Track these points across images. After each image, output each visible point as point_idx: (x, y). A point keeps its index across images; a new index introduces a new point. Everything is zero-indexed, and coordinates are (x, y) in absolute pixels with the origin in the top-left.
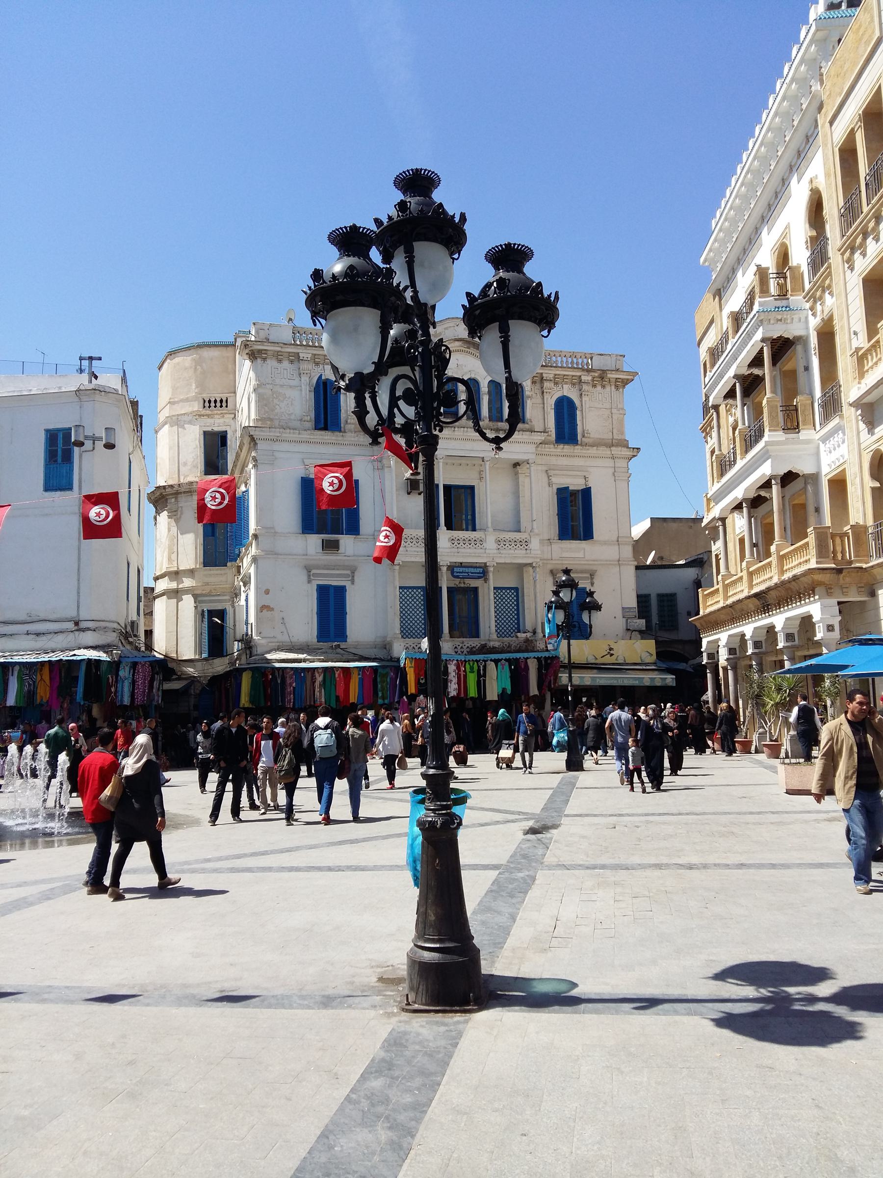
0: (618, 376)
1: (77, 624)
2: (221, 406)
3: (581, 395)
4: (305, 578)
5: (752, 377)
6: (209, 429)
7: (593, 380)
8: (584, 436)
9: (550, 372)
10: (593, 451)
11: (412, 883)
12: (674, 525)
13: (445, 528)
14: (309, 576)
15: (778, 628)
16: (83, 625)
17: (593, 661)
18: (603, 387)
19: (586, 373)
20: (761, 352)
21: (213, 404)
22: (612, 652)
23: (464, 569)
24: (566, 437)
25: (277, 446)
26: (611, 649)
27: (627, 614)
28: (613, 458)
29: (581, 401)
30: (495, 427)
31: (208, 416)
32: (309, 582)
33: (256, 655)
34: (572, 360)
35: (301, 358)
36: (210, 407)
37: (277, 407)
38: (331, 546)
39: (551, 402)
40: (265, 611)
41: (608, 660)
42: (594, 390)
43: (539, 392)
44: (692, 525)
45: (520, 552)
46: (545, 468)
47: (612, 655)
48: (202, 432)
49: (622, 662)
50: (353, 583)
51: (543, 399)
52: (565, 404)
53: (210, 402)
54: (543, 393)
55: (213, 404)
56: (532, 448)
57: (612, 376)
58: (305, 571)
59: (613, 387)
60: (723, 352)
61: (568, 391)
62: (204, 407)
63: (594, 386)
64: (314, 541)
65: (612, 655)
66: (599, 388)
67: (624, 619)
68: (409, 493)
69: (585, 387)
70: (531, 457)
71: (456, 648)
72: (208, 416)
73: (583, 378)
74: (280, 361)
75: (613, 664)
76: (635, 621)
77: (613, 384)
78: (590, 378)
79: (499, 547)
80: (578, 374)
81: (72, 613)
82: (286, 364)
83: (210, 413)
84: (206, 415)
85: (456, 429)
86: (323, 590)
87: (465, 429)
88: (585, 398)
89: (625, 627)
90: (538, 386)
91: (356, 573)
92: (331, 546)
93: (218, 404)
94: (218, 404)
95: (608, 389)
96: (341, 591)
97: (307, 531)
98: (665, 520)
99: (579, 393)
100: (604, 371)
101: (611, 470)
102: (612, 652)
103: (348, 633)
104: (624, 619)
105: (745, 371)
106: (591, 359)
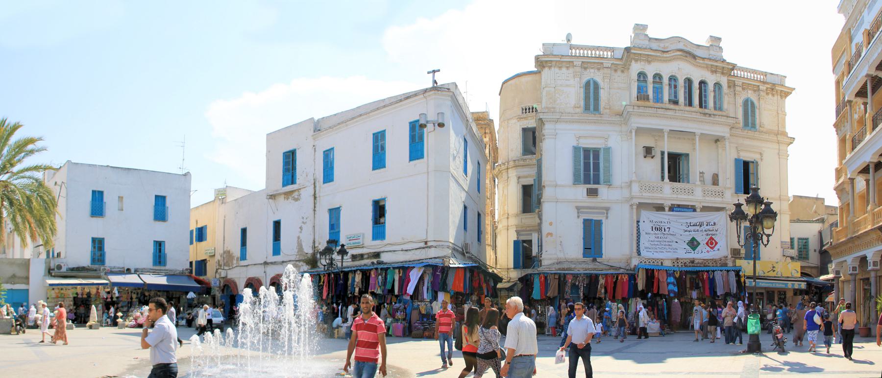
0: (783, 89)
1: (426, 243)
2: (533, 112)
3: (759, 98)
4: (576, 215)
5: (878, 78)
6: (526, 127)
7: (767, 90)
8: (760, 126)
9: (740, 80)
10: (766, 136)
11: (876, 66)
12: (806, 201)
13: (668, 180)
14: (578, 213)
15: (870, 258)
16: (429, 244)
17: (762, 275)
18: (773, 95)
19: (763, 84)
20: (865, 85)
21: (527, 111)
22: (774, 269)
23: (681, 209)
24: (750, 125)
25: (559, 126)
26: (774, 267)
27: (784, 246)
28: (778, 143)
29: (759, 103)
30: (703, 112)
31: (524, 118)
32: (578, 217)
33: (544, 266)
34: (754, 76)
35: (575, 65)
36: (526, 113)
37: (558, 99)
38: (592, 193)
39: (740, 101)
40: (549, 236)
41: (772, 274)
42: (766, 96)
43: (732, 94)
44: (815, 201)
45: (719, 199)
46: (736, 145)
47: (774, 271)
48: (521, 129)
49: (780, 275)
50: (607, 218)
51: (735, 98)
52: (749, 103)
53: (526, 109)
54: (735, 94)
55: (527, 111)
56: (727, 129)
57: (779, 88)
58: (576, 210)
59: (779, 96)
60: (873, 37)
61: (751, 95)
62: (523, 113)
63: (767, 94)
64: (582, 189)
65: (774, 271)
66: (770, 96)
67: (782, 249)
68: (645, 157)
69: (762, 93)
70: (727, 135)
71: (674, 263)
72: (524, 118)
73: (761, 87)
74: (560, 68)
75: (775, 277)
76: (788, 250)
77: (779, 94)
78: (765, 88)
79: (704, 195)
80: (758, 84)
81: (424, 238)
82: (564, 70)
83: (526, 116)
84: (524, 118)
85: (677, 111)
86: (587, 223)
87: (683, 112)
88: (761, 102)
89: (782, 255)
90: (732, 90)
91: (609, 212)
92: (592, 193)
93: (531, 110)
94: (531, 110)
95: (776, 97)
96: (599, 223)
97: (576, 183)
98: (801, 197)
99: (758, 98)
100: (774, 85)
101: (777, 151)
102: (774, 269)
103: (603, 252)
104: (782, 249)
105: (873, 73)
106: (766, 76)
